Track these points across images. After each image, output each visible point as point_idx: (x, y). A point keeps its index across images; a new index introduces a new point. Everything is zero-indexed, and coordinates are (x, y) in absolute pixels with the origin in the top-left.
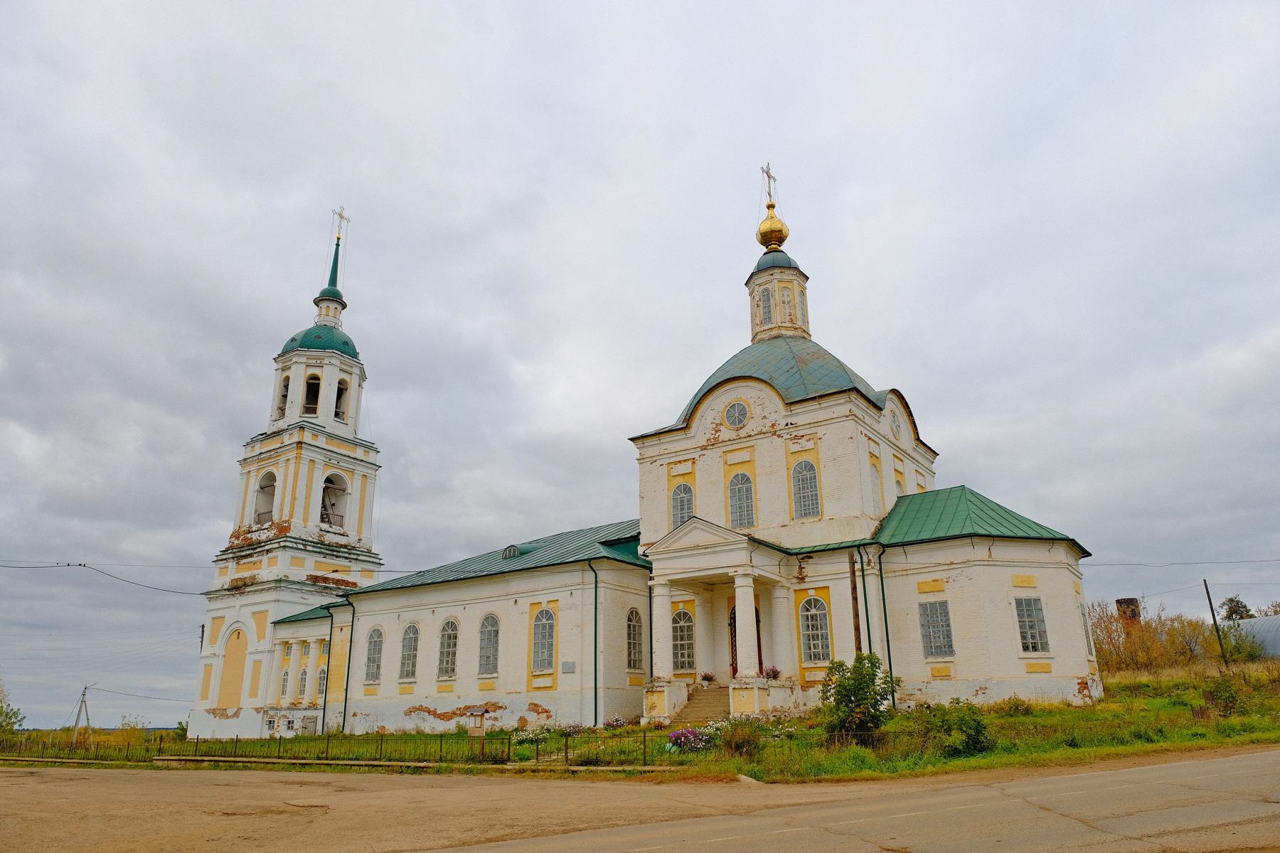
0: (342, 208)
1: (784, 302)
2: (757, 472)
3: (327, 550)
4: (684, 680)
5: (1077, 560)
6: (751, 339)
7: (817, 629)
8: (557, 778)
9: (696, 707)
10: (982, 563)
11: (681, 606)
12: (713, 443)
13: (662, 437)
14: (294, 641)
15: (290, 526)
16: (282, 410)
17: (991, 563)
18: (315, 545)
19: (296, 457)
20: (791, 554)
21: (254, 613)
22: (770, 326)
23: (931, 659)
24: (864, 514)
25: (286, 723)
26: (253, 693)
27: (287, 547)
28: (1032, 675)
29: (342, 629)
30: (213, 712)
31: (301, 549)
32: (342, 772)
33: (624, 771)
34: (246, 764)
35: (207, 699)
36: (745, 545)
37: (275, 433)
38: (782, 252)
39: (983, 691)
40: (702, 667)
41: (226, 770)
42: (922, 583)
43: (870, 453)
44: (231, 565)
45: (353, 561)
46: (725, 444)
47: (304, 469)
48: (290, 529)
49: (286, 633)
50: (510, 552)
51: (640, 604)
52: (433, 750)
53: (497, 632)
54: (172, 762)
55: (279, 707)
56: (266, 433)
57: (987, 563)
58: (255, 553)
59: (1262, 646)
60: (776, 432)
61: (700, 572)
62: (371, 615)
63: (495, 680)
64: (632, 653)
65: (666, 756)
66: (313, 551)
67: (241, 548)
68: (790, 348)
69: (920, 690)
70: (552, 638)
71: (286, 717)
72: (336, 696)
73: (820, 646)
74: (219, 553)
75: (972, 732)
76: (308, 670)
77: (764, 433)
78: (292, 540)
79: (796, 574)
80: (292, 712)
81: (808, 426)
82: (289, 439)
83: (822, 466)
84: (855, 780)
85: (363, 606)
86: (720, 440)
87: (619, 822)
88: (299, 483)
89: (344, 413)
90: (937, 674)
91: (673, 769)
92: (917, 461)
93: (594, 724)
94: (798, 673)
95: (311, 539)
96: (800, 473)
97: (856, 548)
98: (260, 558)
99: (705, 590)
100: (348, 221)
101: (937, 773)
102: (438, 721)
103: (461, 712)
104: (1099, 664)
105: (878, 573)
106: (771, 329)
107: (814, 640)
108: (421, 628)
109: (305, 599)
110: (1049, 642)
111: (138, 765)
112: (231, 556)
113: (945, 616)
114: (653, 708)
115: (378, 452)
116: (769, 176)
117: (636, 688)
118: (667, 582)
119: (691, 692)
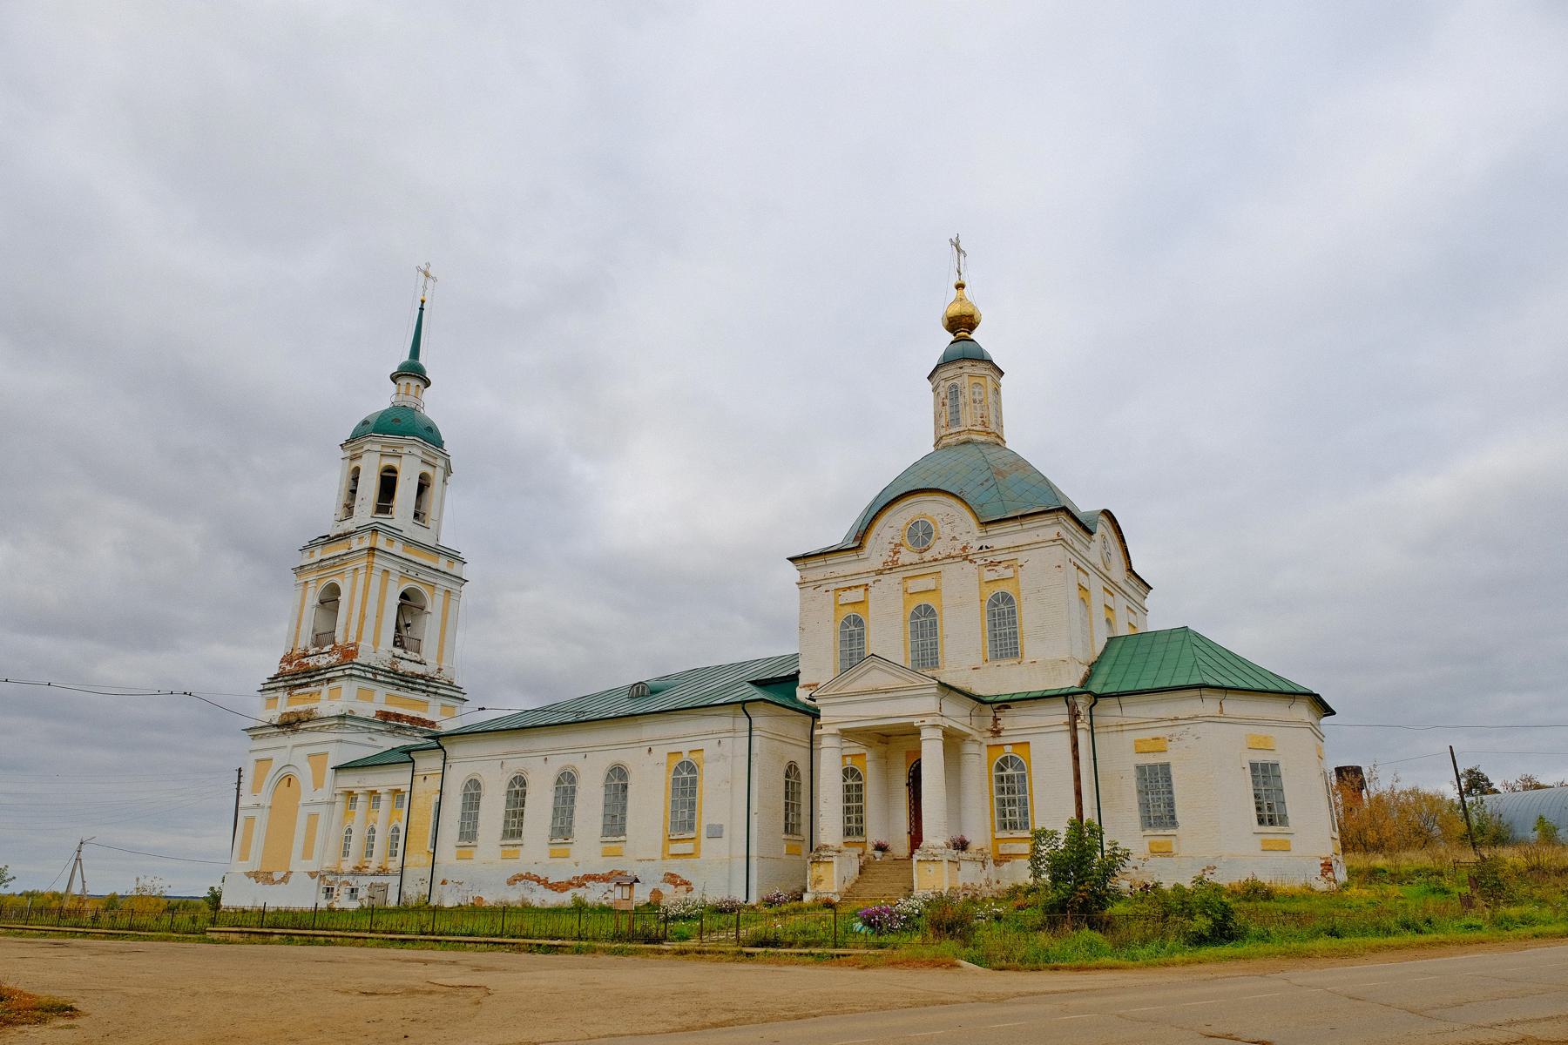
0: (428, 265)
1: (975, 401)
3: (401, 680)
4: (855, 849)
5: (1319, 719)
6: (933, 443)
7: (1014, 792)
8: (729, 961)
9: (869, 882)
10: (1213, 719)
11: (849, 760)
12: (891, 567)
13: (828, 557)
14: (361, 791)
16: (349, 509)
17: (1222, 720)
18: (387, 674)
19: (367, 566)
20: (985, 703)
21: (309, 756)
22: (957, 429)
23: (1149, 832)
24: (1072, 658)
25: (348, 891)
26: (307, 854)
27: (354, 675)
28: (1268, 853)
29: (425, 778)
30: (255, 875)
31: (370, 679)
32: (455, 949)
33: (812, 955)
34: (329, 939)
35: (247, 859)
36: (935, 690)
37: (339, 536)
38: (972, 340)
40: (873, 834)
41: (303, 945)
42: (1140, 741)
43: (1079, 584)
44: (282, 695)
45: (432, 695)
46: (905, 568)
47: (376, 580)
48: (357, 654)
49: (350, 781)
50: (638, 691)
51: (800, 757)
52: (569, 925)
53: (625, 787)
54: (232, 934)
55: (339, 872)
56: (328, 536)
57: (1217, 719)
58: (313, 682)
59: (1510, 827)
60: (967, 556)
61: (881, 721)
62: (466, 762)
63: (624, 844)
64: (790, 815)
65: (860, 939)
66: (384, 682)
67: (294, 675)
68: (981, 452)
70: (695, 795)
71: (348, 884)
73: (1017, 813)
74: (267, 681)
75: (1219, 917)
76: (377, 827)
77: (953, 557)
78: (359, 667)
79: (990, 726)
81: (1007, 551)
82: (358, 544)
84: (1097, 969)
85: (456, 751)
87: (856, 1008)
88: (370, 597)
89: (424, 514)
91: (871, 952)
92: (1129, 596)
93: (745, 899)
94: (990, 844)
95: (382, 667)
96: (995, 605)
97: (1063, 698)
98: (318, 688)
99: (879, 742)
100: (435, 280)
101: (1189, 963)
102: (550, 892)
103: (581, 882)
104: (1343, 844)
105: (1088, 727)
106: (959, 432)
107: (1009, 806)
108: (529, 778)
109: (373, 740)
111: (187, 938)
112: (281, 684)
113: (1166, 781)
114: (818, 881)
115: (465, 563)
116: (957, 246)
117: (793, 857)
118: (838, 732)
119: (862, 864)
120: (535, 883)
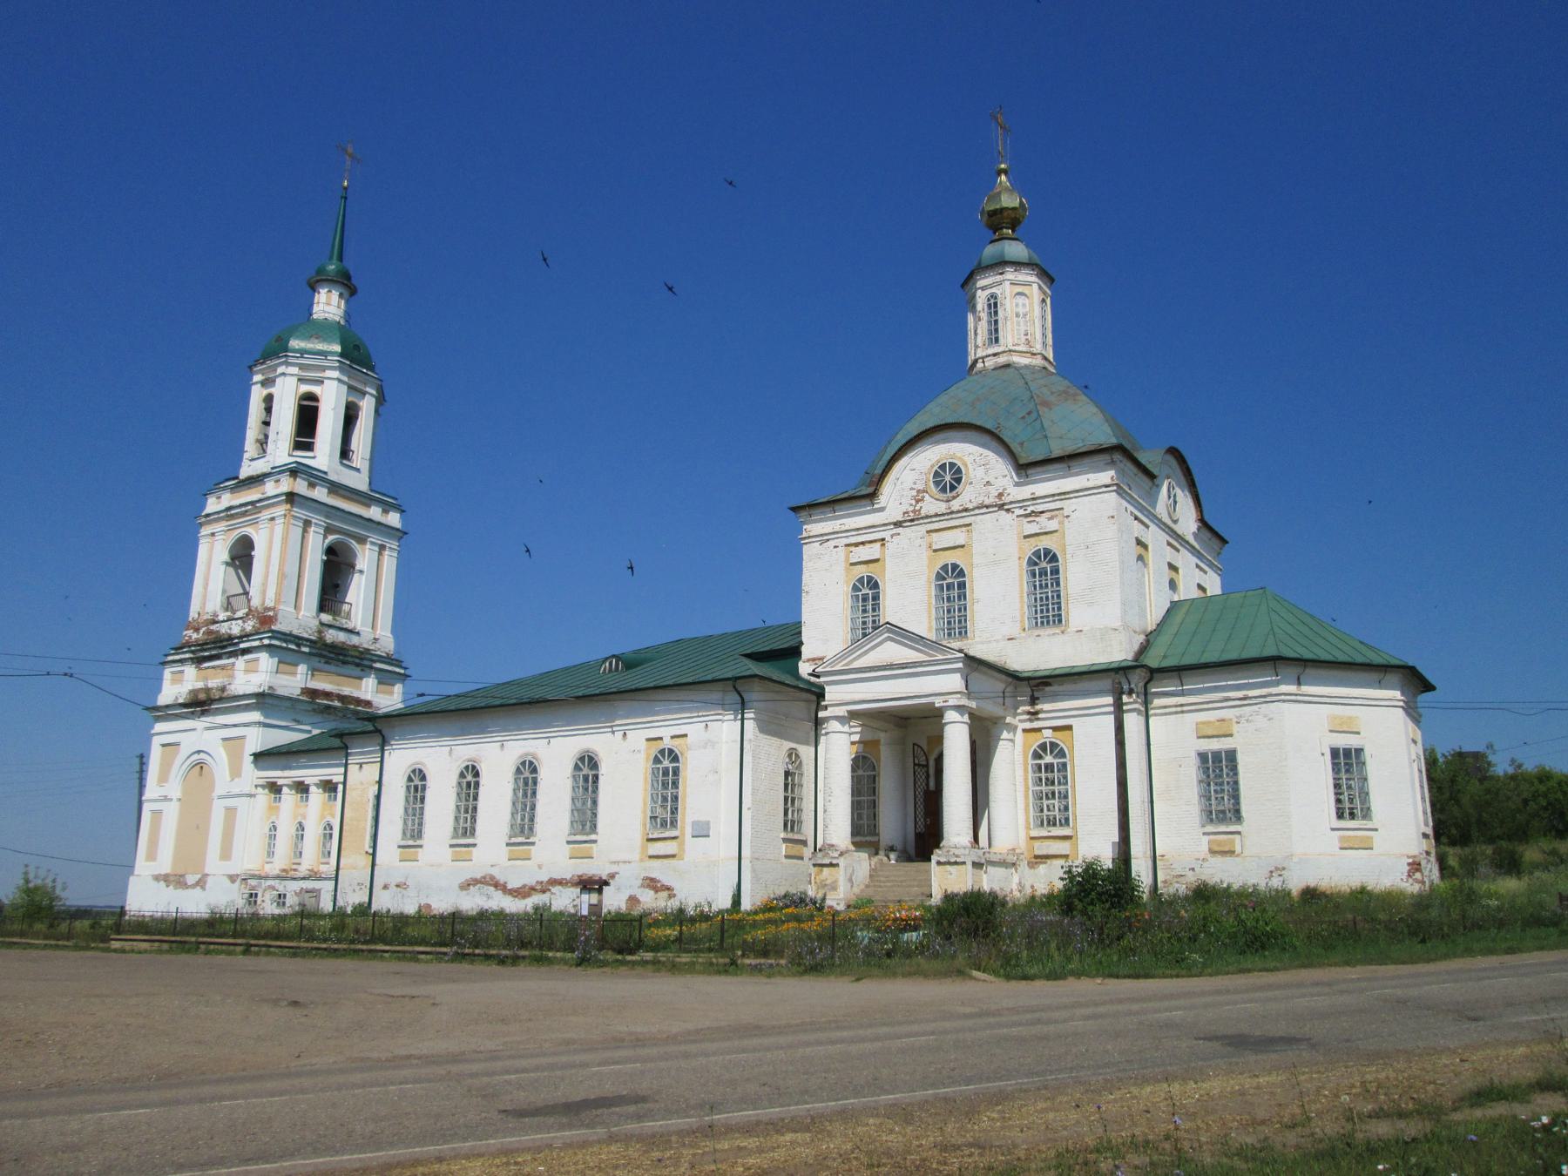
2: (975, 561)
5: (1415, 696)
15: (276, 615)
21: (224, 739)
23: (1210, 828)
26: (226, 854)
30: (165, 879)
31: (293, 650)
36: (960, 665)
39: (1279, 872)
48: (276, 620)
69: (1193, 869)
70: (677, 788)
71: (273, 888)
72: (355, 863)
80: (283, 882)
83: (1068, 556)
86: (923, 515)
90: (1216, 849)
95: (306, 635)
98: (232, 660)
110: (1372, 808)
119: (873, 867)
120: (492, 888)
